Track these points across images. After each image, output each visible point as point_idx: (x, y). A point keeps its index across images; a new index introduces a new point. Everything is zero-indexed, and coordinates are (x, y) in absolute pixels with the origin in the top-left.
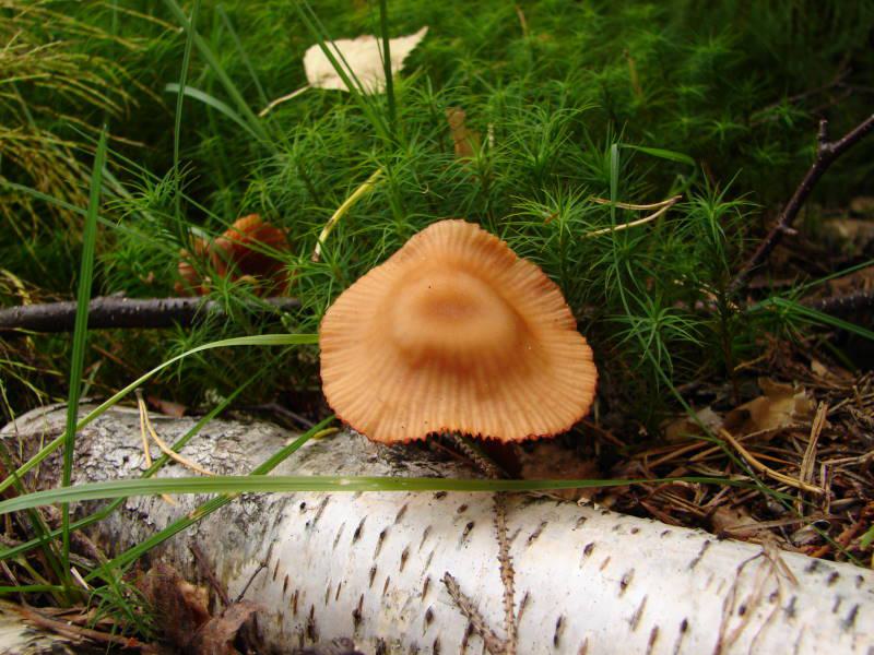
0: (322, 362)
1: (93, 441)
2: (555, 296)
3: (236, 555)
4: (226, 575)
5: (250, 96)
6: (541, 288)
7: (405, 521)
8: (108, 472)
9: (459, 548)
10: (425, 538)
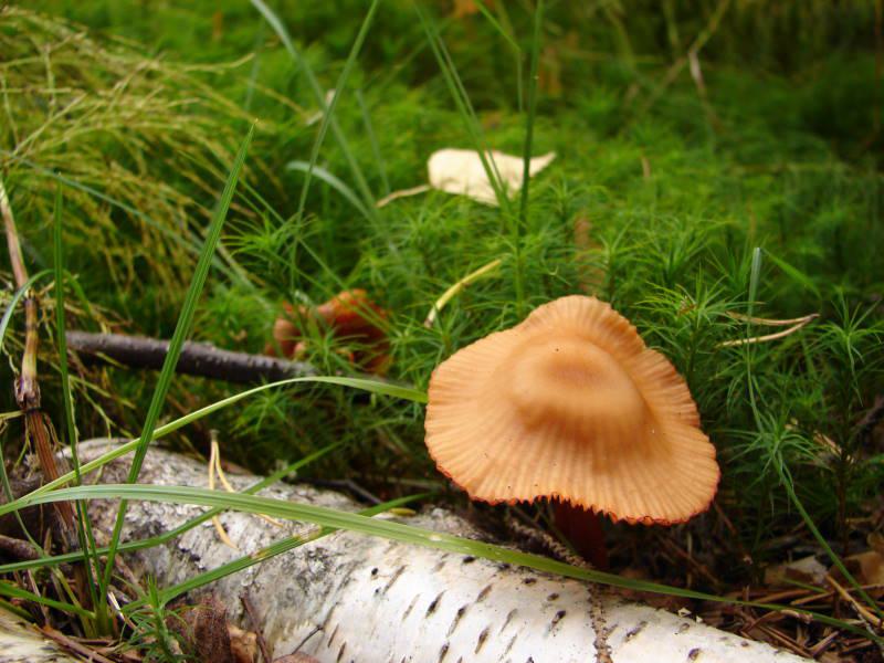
0: (428, 413)
1: (155, 476)
2: (681, 390)
3: (290, 613)
4: (274, 634)
5: (375, 186)
6: (668, 380)
7: (487, 601)
8: (166, 508)
9: (546, 636)
10: (508, 621)
